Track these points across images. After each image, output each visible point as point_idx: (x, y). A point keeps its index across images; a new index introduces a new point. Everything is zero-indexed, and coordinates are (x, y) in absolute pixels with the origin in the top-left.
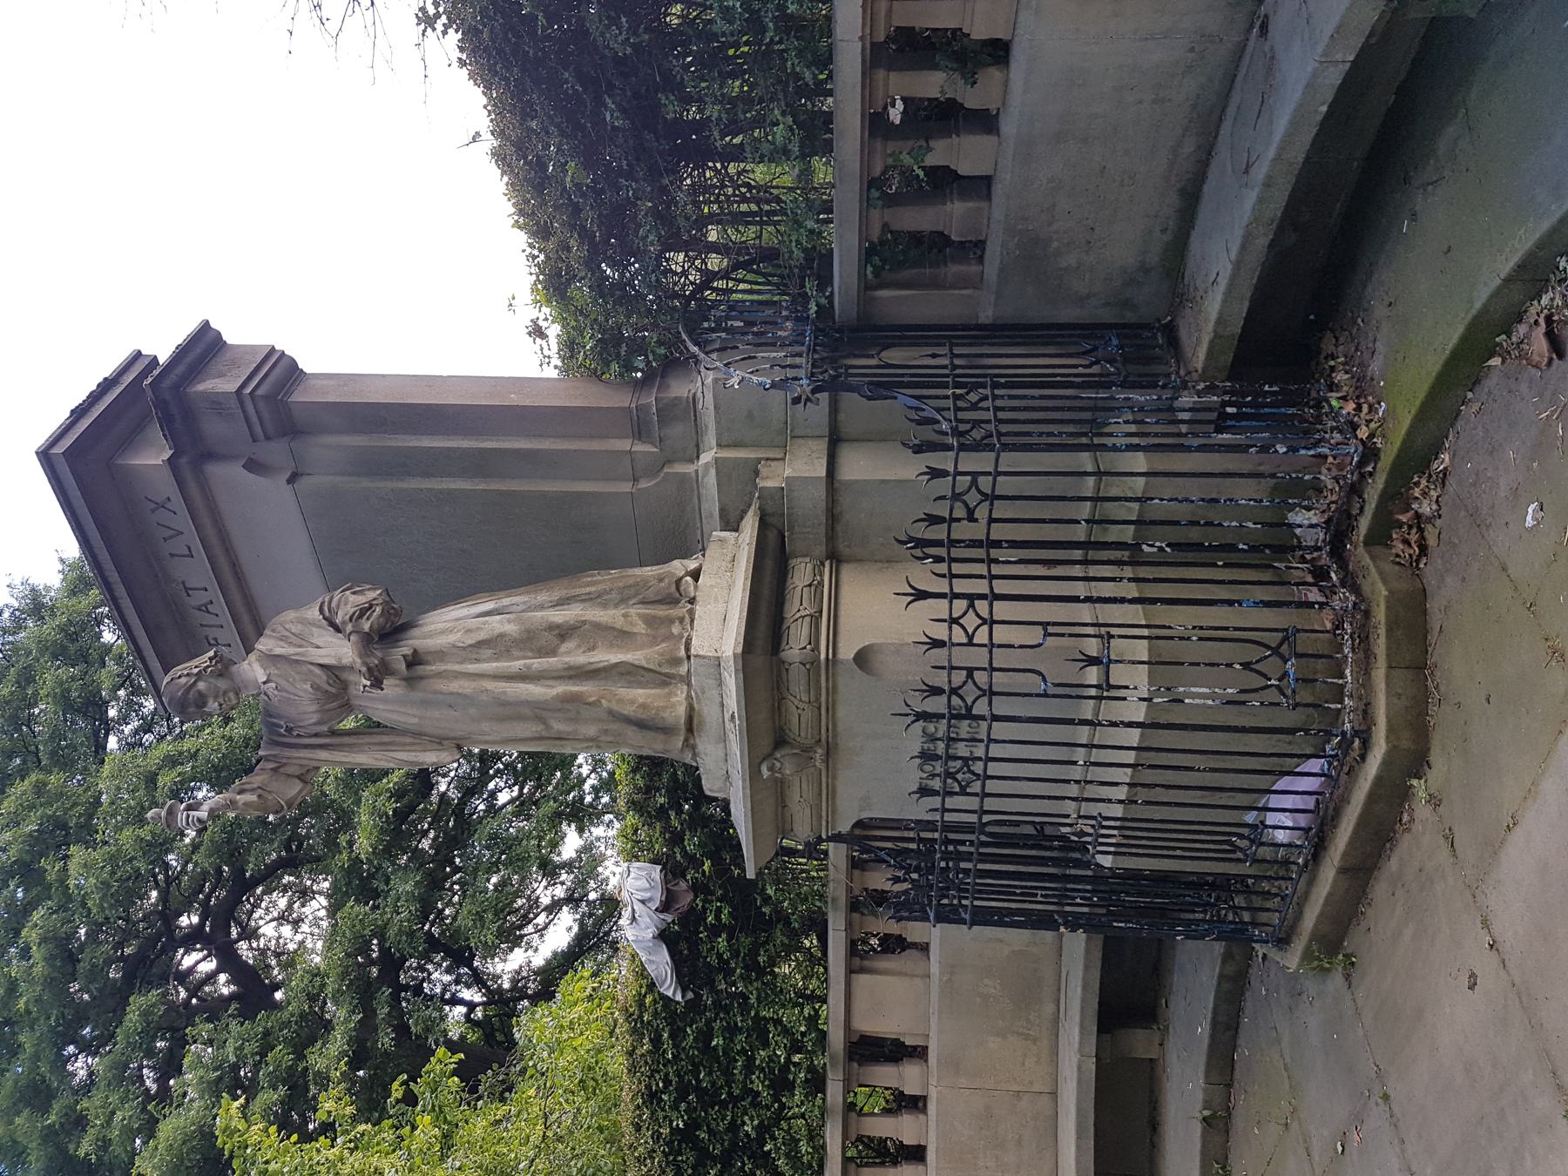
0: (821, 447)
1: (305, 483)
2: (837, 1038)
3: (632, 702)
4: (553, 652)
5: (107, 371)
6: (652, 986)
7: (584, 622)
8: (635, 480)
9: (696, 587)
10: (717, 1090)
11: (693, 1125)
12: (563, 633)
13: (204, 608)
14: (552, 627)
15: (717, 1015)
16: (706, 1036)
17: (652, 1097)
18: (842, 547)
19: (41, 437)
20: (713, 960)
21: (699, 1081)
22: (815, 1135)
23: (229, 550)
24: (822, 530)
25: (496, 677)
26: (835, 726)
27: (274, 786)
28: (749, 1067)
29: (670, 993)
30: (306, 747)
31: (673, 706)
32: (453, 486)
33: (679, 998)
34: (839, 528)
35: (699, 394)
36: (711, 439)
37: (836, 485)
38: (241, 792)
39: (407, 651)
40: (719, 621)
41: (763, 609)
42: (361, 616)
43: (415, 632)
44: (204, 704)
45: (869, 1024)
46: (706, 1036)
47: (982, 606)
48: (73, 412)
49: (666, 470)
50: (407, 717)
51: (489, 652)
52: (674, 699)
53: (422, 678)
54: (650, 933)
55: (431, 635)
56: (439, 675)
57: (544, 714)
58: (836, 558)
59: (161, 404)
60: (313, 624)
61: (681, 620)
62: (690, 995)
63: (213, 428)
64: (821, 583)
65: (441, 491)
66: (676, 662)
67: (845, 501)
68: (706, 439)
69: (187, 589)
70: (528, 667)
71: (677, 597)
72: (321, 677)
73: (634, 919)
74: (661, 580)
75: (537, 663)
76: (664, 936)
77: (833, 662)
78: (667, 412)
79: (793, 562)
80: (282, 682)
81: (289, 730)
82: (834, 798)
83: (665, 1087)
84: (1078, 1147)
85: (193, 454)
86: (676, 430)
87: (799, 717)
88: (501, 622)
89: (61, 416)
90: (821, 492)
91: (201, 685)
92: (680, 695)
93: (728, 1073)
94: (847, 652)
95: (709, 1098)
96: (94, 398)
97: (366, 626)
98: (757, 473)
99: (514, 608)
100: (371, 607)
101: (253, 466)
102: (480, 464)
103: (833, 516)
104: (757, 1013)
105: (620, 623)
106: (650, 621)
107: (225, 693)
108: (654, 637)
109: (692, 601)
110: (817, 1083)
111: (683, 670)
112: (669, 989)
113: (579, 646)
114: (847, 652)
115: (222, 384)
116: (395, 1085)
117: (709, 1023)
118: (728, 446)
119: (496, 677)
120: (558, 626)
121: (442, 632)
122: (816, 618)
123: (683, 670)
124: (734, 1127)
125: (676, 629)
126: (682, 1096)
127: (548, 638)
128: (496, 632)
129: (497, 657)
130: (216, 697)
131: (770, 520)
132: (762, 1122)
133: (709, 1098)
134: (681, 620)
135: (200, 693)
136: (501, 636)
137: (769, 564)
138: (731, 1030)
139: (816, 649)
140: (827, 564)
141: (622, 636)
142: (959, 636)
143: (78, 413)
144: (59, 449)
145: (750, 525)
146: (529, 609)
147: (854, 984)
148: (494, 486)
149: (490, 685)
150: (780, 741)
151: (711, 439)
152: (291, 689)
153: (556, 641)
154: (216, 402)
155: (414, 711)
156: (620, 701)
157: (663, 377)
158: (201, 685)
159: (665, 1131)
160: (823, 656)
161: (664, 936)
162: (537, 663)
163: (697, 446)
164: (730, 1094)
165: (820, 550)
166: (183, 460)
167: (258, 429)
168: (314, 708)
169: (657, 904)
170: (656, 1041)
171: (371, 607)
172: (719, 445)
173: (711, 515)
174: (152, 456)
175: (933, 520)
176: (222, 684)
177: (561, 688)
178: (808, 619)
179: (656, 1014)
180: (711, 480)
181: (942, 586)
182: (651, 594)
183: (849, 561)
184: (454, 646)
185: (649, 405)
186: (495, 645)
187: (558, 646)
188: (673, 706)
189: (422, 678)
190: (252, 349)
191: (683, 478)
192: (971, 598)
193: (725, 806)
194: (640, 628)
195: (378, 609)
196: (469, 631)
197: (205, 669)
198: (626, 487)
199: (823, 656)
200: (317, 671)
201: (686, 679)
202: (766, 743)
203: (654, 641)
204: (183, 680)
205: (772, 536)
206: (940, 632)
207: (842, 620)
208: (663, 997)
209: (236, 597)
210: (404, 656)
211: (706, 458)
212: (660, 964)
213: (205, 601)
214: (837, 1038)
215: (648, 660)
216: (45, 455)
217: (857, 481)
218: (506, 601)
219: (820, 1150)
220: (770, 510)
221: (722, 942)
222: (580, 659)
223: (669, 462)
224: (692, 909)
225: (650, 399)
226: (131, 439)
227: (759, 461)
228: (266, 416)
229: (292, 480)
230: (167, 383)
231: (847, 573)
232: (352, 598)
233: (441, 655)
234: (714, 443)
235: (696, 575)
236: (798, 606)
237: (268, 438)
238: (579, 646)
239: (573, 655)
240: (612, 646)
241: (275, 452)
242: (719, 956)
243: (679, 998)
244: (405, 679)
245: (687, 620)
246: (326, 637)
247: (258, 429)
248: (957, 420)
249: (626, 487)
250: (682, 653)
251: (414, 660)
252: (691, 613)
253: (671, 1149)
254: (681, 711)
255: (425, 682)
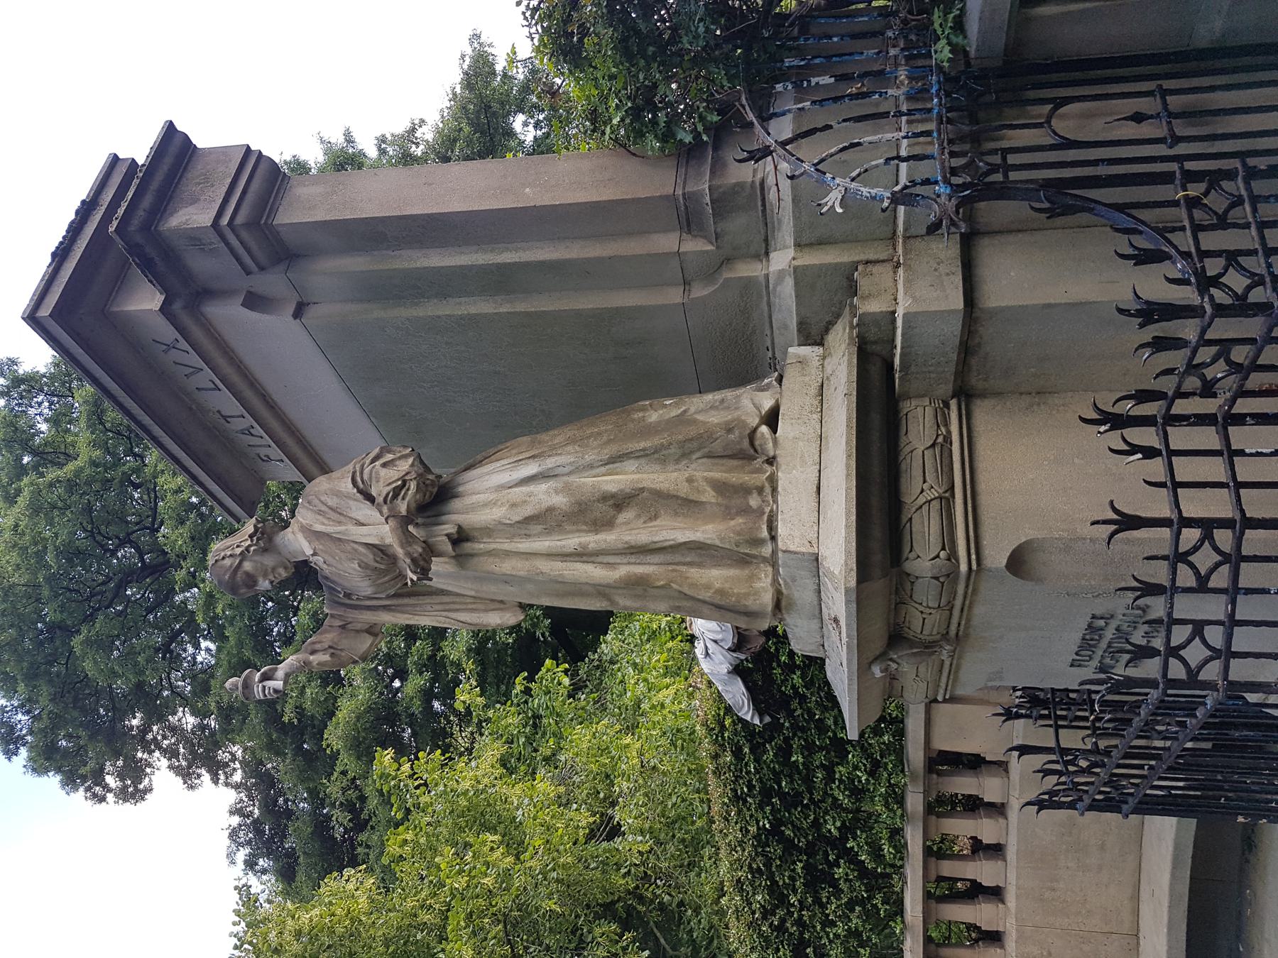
0: (946, 250)
1: (312, 313)
2: (915, 754)
3: (707, 587)
4: (609, 524)
5: (82, 191)
6: (729, 710)
7: (642, 490)
8: (686, 283)
9: (775, 442)
10: (799, 795)
11: (777, 824)
12: (619, 501)
13: (248, 432)
14: (605, 497)
15: (795, 735)
16: (784, 752)
17: (737, 798)
18: (975, 381)
19: (23, 299)
20: (789, 691)
21: (780, 787)
22: (896, 833)
23: (253, 384)
24: (951, 368)
25: (551, 555)
26: (968, 620)
27: (344, 643)
28: (830, 778)
29: (748, 718)
30: (369, 608)
31: (757, 593)
32: (473, 310)
33: (757, 721)
34: (974, 361)
35: (771, 180)
36: (786, 234)
37: (977, 314)
38: (313, 652)
39: (450, 529)
40: (816, 512)
41: (875, 501)
42: (395, 496)
43: (456, 504)
44: (255, 583)
45: (943, 743)
46: (784, 752)
47: (1224, 538)
48: (54, 255)
49: (727, 274)
50: (466, 588)
51: (539, 528)
52: (758, 585)
53: (472, 555)
54: (725, 668)
55: (473, 508)
56: (489, 553)
57: (607, 590)
58: (965, 394)
59: (133, 248)
60: (348, 497)
61: (760, 490)
62: (767, 719)
63: (202, 265)
64: (948, 439)
65: (462, 317)
66: (759, 542)
67: (987, 331)
68: (779, 235)
69: (225, 417)
70: (584, 546)
71: (749, 450)
72: (369, 557)
73: (707, 654)
74: (729, 431)
75: (593, 540)
76: (738, 670)
77: (978, 569)
78: (725, 202)
79: (906, 406)
80: (330, 559)
81: (348, 595)
82: (957, 672)
83: (749, 790)
84: (1173, 875)
85: (187, 295)
86: (739, 225)
87: (923, 618)
88: (547, 492)
89: (42, 262)
90: (954, 328)
91: (247, 566)
92: (764, 582)
93: (808, 780)
94: (997, 557)
95: (792, 801)
96: (75, 230)
97: (403, 508)
98: (852, 289)
99: (560, 470)
100: (404, 482)
101: (254, 301)
102: (500, 280)
103: (967, 348)
104: (835, 734)
105: (684, 490)
106: (721, 488)
107: (274, 569)
108: (727, 507)
109: (771, 461)
110: (896, 797)
111: (767, 550)
112: (747, 713)
113: (638, 516)
114: (997, 557)
115: (193, 215)
116: (518, 680)
117: (787, 740)
118: (811, 245)
119: (551, 555)
120: (613, 496)
121: (486, 505)
122: (946, 501)
123: (767, 550)
124: (816, 824)
125: (754, 501)
126: (767, 794)
127: (603, 509)
128: (544, 506)
129: (549, 531)
130: (265, 576)
131: (870, 348)
132: (843, 823)
133: (792, 801)
134: (760, 490)
135: (247, 574)
136: (550, 510)
137: (876, 419)
138: (809, 749)
139: (953, 556)
140: (953, 403)
141: (686, 505)
142: (1185, 577)
143: (60, 255)
144: (44, 312)
145: (841, 339)
146: (578, 470)
147: (933, 712)
148: (521, 307)
149: (546, 566)
150: (896, 638)
151: (786, 234)
152: (340, 566)
153: (612, 512)
154: (194, 237)
155: (469, 585)
156: (693, 585)
157: (716, 148)
158: (247, 566)
159: (753, 829)
160: (963, 567)
161: (738, 670)
162: (593, 540)
163: (766, 240)
164: (811, 799)
165: (946, 388)
166: (177, 306)
167: (247, 260)
168: (367, 583)
169: (730, 644)
170: (738, 753)
171: (404, 482)
172: (798, 245)
173: (786, 327)
174: (145, 301)
175: (1143, 396)
176: (269, 561)
177: (623, 571)
178: (936, 504)
179: (736, 733)
180: (787, 290)
181: (1159, 506)
182: (717, 447)
183: (983, 395)
184: (500, 523)
185: (700, 194)
186: (545, 520)
187: (614, 517)
188: (757, 593)
189: (472, 555)
190: (225, 151)
191: (748, 285)
192: (1208, 526)
193: (815, 664)
194: (709, 496)
195: (413, 485)
196: (514, 505)
197: (247, 549)
198: (674, 296)
199: (963, 567)
200: (361, 549)
201: (773, 561)
202: (878, 645)
203: (728, 514)
204: (227, 562)
205: (875, 370)
206: (1159, 573)
207: (983, 500)
208: (741, 720)
209: (274, 424)
210: (448, 535)
211: (782, 259)
212: (736, 693)
213: (245, 426)
214: (915, 754)
215: (722, 540)
216: (32, 318)
217: (1008, 308)
218: (550, 463)
219: (901, 849)
220: (871, 336)
221: (796, 679)
222: (642, 536)
223: (728, 261)
224: (765, 649)
225: (702, 185)
226: (118, 283)
227: (855, 267)
228: (253, 245)
229: (298, 314)
230: (136, 223)
231: (983, 414)
232: (383, 472)
233: (488, 531)
234: (790, 241)
235: (772, 420)
236: (919, 487)
237: (262, 269)
238: (638, 516)
239: (632, 530)
240: (676, 514)
241: (272, 282)
242: (793, 687)
243: (757, 721)
244: (454, 557)
245: (768, 490)
246: (364, 511)
247: (247, 260)
248: (1204, 254)
249: (674, 296)
250: (765, 533)
251: (461, 538)
252: (773, 480)
253: (759, 842)
254: (767, 599)
255: (476, 560)
